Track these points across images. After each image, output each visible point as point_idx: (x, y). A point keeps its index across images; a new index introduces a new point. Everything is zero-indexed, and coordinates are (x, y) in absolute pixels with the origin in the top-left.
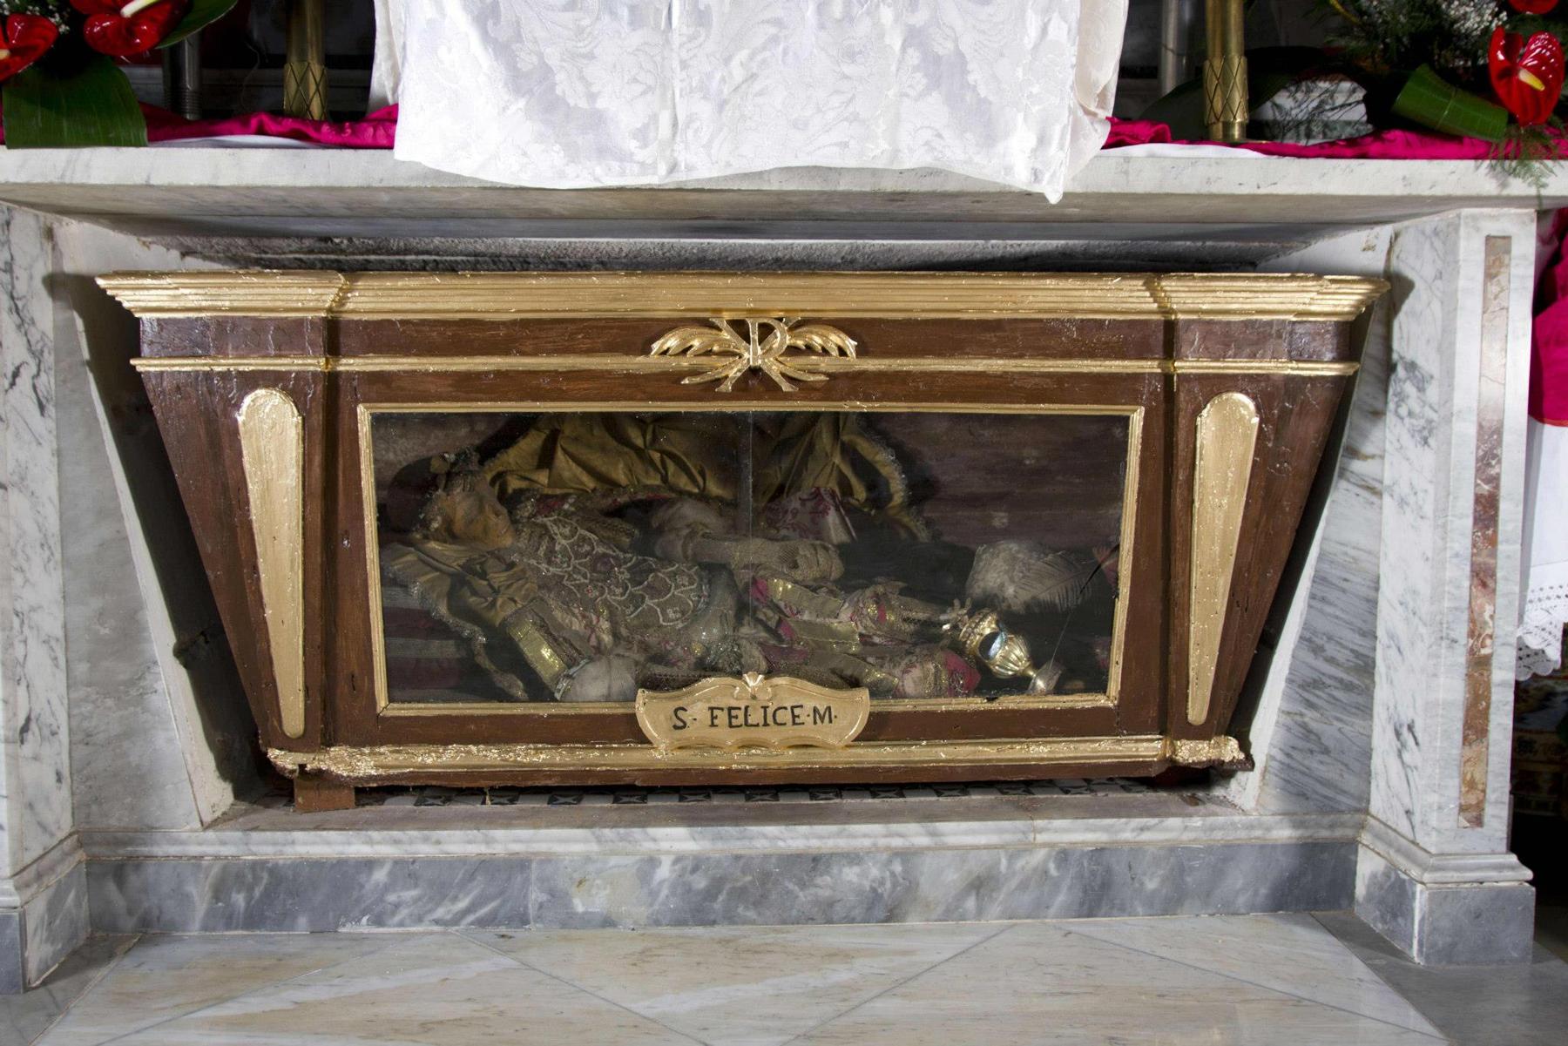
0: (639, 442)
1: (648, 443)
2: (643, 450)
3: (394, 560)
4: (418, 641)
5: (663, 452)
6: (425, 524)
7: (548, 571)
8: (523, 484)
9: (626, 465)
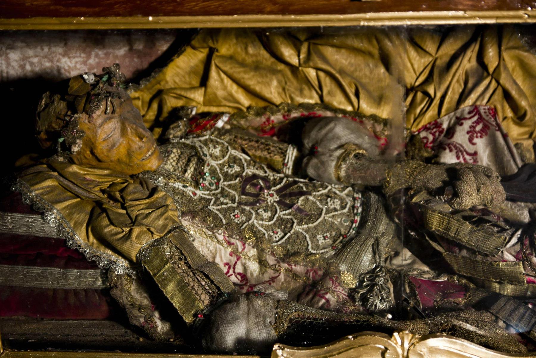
0: (295, 61)
1: (302, 61)
2: (297, 68)
3: (33, 185)
4: (56, 270)
5: (318, 69)
6: (67, 148)
7: (195, 194)
8: (180, 103)
9: (279, 82)
